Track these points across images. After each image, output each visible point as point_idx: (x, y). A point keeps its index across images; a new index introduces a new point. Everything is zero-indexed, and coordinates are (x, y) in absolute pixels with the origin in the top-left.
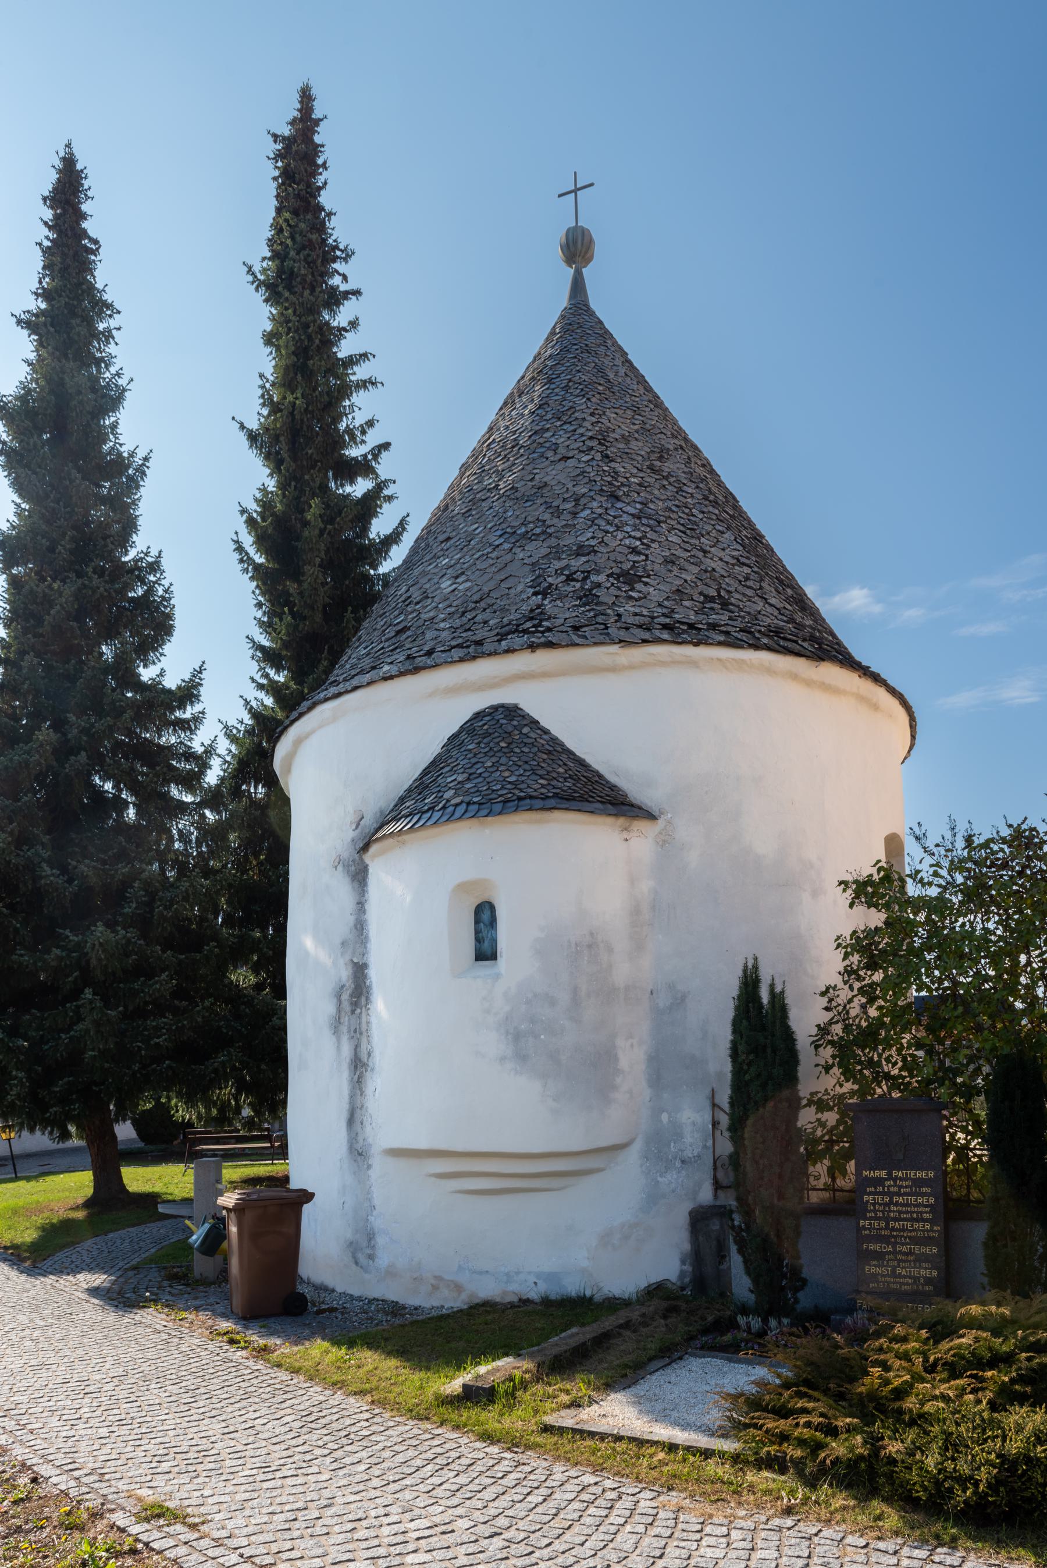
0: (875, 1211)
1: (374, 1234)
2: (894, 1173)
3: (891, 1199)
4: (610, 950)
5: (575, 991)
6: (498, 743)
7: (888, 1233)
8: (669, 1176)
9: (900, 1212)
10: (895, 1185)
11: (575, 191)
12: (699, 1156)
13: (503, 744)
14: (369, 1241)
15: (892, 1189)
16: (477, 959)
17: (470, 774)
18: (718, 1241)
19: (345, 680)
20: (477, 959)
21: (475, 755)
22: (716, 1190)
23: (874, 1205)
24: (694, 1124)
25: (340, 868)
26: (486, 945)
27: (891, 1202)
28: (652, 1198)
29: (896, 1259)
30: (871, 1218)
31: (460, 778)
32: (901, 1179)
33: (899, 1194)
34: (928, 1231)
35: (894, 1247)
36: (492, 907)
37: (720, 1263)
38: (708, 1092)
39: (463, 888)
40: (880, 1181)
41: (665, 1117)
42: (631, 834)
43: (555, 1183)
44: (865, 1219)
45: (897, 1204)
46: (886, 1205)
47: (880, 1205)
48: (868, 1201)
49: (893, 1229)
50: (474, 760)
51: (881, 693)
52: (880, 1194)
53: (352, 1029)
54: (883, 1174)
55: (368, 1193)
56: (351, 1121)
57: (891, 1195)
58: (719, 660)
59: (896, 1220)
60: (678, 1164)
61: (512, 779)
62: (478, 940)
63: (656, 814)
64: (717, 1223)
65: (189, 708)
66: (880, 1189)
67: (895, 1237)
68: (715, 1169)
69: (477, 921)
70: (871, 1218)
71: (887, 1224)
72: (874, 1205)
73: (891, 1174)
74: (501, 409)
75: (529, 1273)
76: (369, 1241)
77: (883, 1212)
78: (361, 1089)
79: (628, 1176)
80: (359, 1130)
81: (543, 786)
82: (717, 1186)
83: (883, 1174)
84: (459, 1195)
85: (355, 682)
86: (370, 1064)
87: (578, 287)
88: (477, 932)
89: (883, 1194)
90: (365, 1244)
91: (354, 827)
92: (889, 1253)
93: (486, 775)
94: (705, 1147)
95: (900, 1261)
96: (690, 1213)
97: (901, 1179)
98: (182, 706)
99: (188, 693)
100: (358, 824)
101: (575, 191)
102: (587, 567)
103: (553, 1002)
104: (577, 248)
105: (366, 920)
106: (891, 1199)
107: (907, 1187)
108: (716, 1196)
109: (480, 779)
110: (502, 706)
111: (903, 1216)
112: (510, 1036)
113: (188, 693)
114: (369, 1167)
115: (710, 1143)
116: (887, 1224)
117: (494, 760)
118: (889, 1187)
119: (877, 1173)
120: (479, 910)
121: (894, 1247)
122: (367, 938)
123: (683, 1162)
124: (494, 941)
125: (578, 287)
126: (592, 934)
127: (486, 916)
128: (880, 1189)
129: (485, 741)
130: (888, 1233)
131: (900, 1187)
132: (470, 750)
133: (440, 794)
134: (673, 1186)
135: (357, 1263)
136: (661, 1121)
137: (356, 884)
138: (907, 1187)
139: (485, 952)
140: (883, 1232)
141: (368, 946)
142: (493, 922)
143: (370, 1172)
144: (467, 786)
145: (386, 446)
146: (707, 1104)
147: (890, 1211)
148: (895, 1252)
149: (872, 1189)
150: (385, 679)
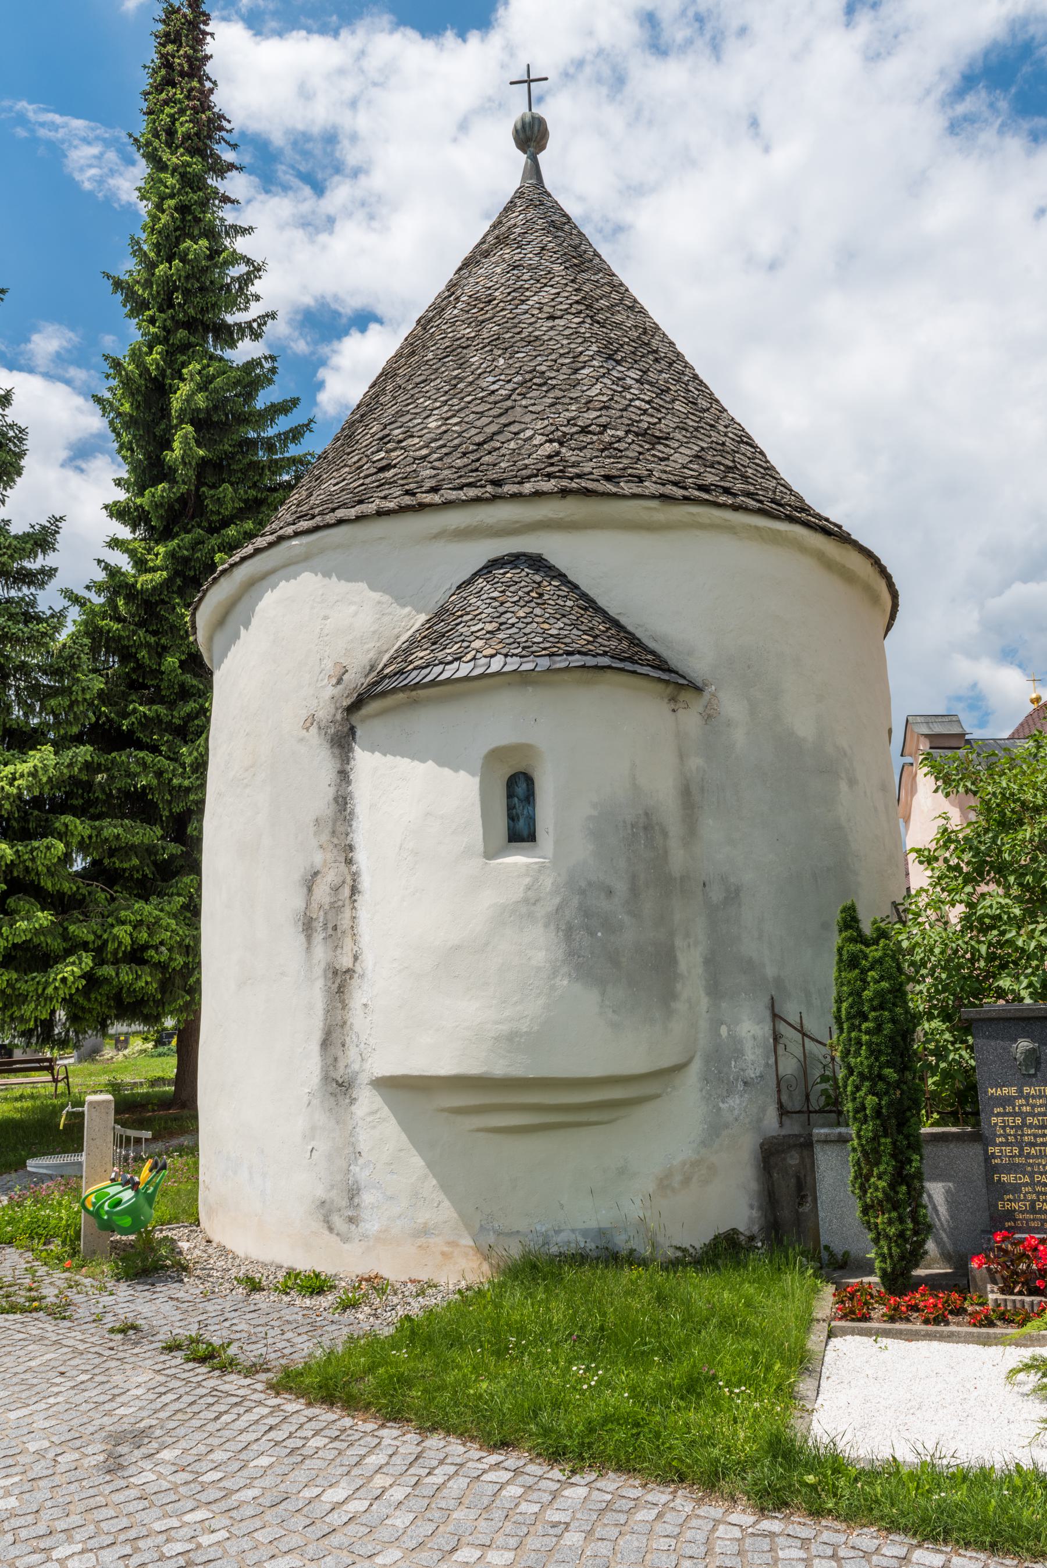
0: (1006, 1136)
1: (359, 1190)
2: (1026, 1090)
3: (1024, 1120)
4: (665, 834)
5: (634, 878)
6: (528, 593)
7: (1022, 1160)
8: (731, 1101)
9: (1036, 1136)
10: (1028, 1104)
11: (529, 81)
12: (761, 1076)
13: (534, 594)
14: (351, 1199)
15: (1024, 1109)
16: (510, 841)
17: (501, 624)
18: (798, 1178)
19: (321, 514)
20: (510, 841)
21: (502, 604)
22: (781, 1115)
23: (1004, 1128)
24: (754, 1038)
25: (314, 730)
26: (521, 824)
27: (1024, 1124)
28: (715, 1128)
29: (1035, 1192)
30: (1001, 1144)
31: (490, 627)
32: (1033, 1097)
33: (1034, 1115)
34: (1015, 1156)
35: (1032, 1177)
36: (529, 780)
37: (800, 1204)
38: (767, 1000)
39: (496, 755)
40: (1008, 1100)
41: (724, 1030)
42: (679, 705)
43: (593, 1117)
44: (995, 1145)
45: (1031, 1126)
46: (1017, 1127)
47: (1012, 1128)
48: (996, 1124)
49: (1029, 1156)
50: (502, 609)
51: (882, 585)
52: (1009, 1114)
53: (330, 926)
54: (1013, 1091)
55: (351, 1135)
56: (326, 1043)
57: (1024, 1115)
58: (757, 528)
59: (1032, 1145)
60: (740, 1086)
61: (554, 632)
62: (512, 817)
63: (700, 685)
64: (797, 1156)
65: (40, 556)
66: (1009, 1109)
67: (1031, 1165)
68: (779, 1091)
69: (510, 795)
70: (1001, 1144)
71: (1021, 1150)
72: (1004, 1128)
73: (1022, 1091)
74: (460, 269)
75: (573, 1231)
76: (351, 1199)
77: (1015, 1136)
78: (342, 1002)
79: (687, 1104)
80: (340, 1053)
81: (589, 643)
82: (783, 1111)
83: (1013, 1091)
84: (481, 1134)
85: (341, 513)
86: (358, 969)
87: (534, 171)
88: (510, 808)
89: (1014, 1114)
90: (344, 1203)
91: (334, 681)
92: (1026, 1184)
93: (520, 625)
94: (767, 1065)
95: (1039, 1193)
96: (762, 1145)
97: (1033, 1097)
98: (32, 554)
99: (42, 539)
100: (339, 681)
101: (529, 81)
102: (603, 420)
103: (610, 893)
104: (531, 136)
105: (350, 793)
106: (1024, 1120)
107: (1041, 1106)
108: (781, 1124)
109: (514, 630)
110: (524, 555)
111: (1039, 1140)
112: (561, 933)
113: (42, 539)
114: (353, 1101)
115: (772, 1061)
116: (1021, 1150)
117: (527, 610)
118: (1020, 1106)
119: (1006, 1091)
120: (512, 782)
121: (1032, 1177)
122: (352, 813)
123: (745, 1083)
124: (532, 820)
125: (534, 171)
126: (647, 814)
127: (521, 789)
128: (1009, 1109)
129: (512, 589)
130: (1022, 1160)
131: (1033, 1106)
132: (494, 598)
133: (465, 644)
134: (736, 1112)
135: (331, 1229)
136: (720, 1035)
137: (337, 751)
138: (1041, 1106)
139: (520, 831)
140: (1017, 1160)
141: (354, 823)
142: (530, 797)
143: (353, 1108)
144: (501, 636)
145: (272, 316)
146: (767, 1014)
147: (1022, 1135)
148: (1033, 1184)
149: (1001, 1110)
150: (380, 513)
